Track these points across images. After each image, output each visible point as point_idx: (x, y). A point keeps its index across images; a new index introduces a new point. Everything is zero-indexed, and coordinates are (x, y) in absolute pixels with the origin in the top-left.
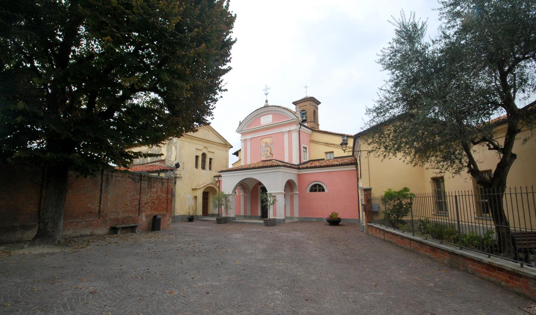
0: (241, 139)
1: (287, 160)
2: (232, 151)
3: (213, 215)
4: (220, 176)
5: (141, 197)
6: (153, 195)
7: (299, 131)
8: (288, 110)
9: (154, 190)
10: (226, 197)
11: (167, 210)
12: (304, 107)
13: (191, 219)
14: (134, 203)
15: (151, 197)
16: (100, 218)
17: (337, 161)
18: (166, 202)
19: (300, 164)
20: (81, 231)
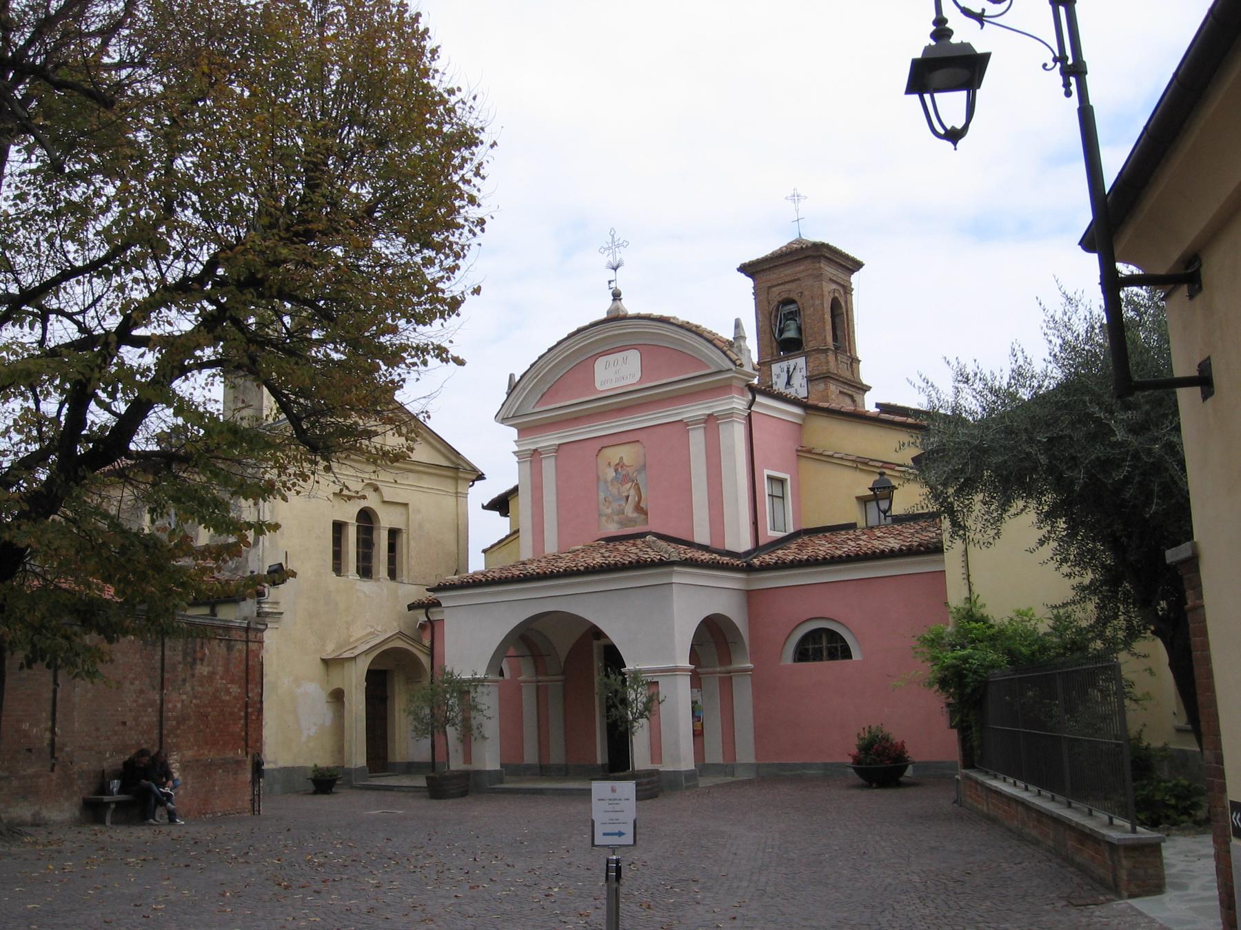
0: (516, 449)
1: (702, 535)
2: (481, 493)
3: (410, 768)
4: (437, 604)
5: (165, 698)
6: (200, 689)
7: (749, 415)
8: (700, 335)
9: (203, 670)
10: (463, 689)
11: (247, 746)
12: (787, 287)
13: (324, 782)
14: (146, 719)
15: (196, 697)
16: (56, 768)
18: (242, 714)
19: (757, 549)
20: (11, 810)
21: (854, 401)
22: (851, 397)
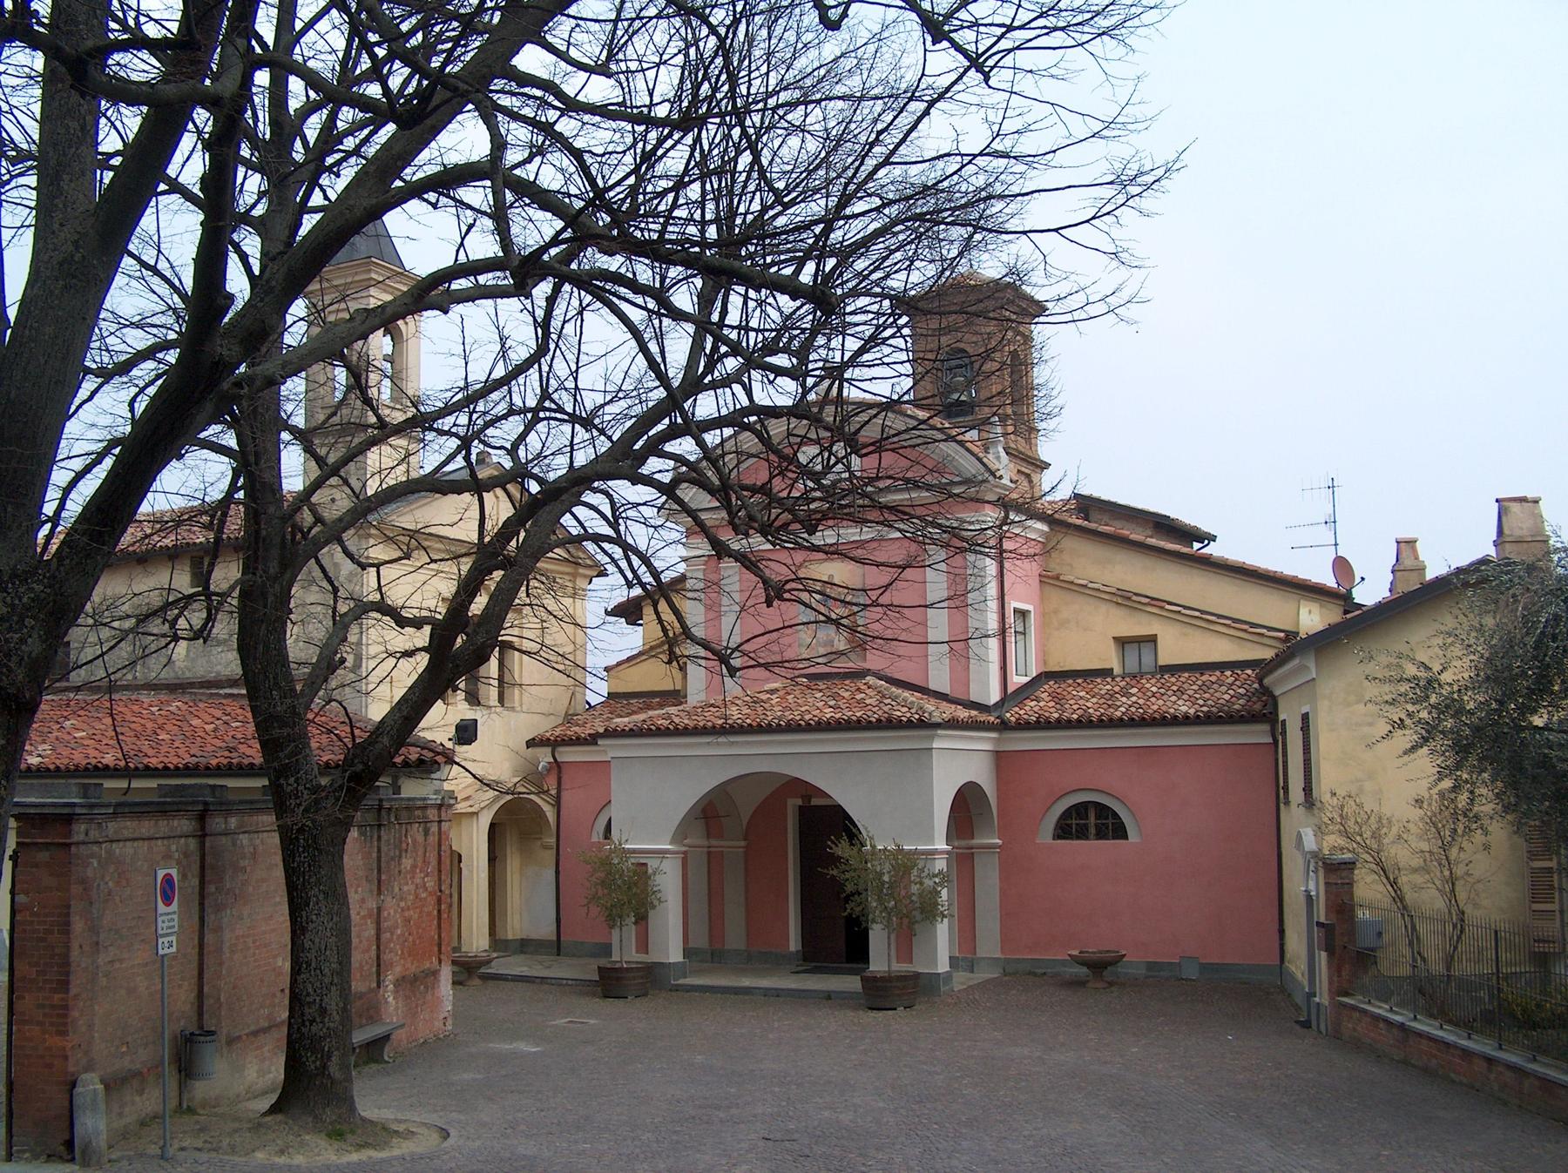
1: (940, 679)
17: (1181, 691)
19: (1006, 698)
21: (1030, 482)
22: (1028, 476)
